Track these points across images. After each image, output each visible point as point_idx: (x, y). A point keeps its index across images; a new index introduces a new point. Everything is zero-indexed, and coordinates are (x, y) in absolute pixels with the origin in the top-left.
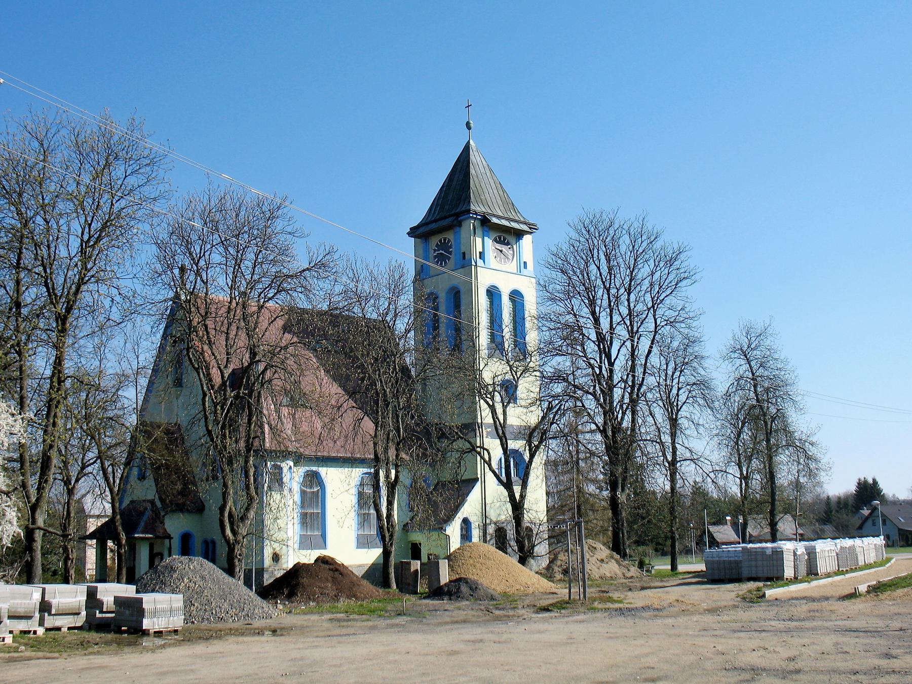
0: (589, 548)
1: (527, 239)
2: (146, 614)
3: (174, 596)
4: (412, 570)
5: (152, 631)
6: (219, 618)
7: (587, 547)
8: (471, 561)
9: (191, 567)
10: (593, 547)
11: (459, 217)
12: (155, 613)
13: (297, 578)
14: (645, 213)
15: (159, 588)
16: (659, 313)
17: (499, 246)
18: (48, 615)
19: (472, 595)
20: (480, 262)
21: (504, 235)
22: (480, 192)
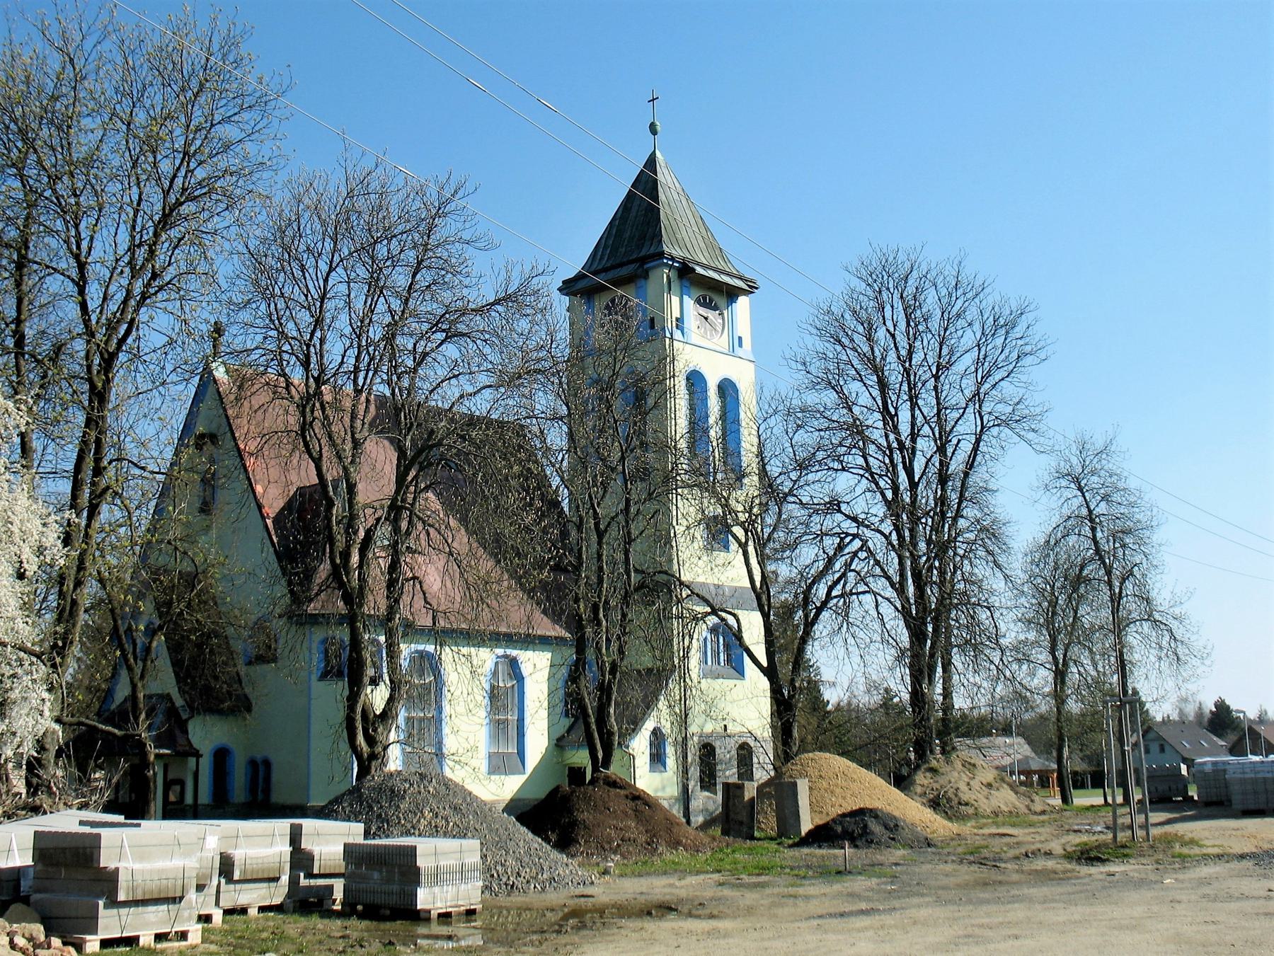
0: (963, 765)
1: (743, 301)
2: (423, 879)
3: (464, 842)
4: (746, 799)
5: (434, 914)
6: (506, 884)
8: (825, 784)
9: (431, 790)
10: (970, 764)
12: (438, 877)
13: (570, 812)
14: (962, 253)
15: (379, 828)
16: (987, 407)
17: (703, 311)
18: (227, 883)
19: (893, 839)
20: (677, 335)
21: (710, 294)
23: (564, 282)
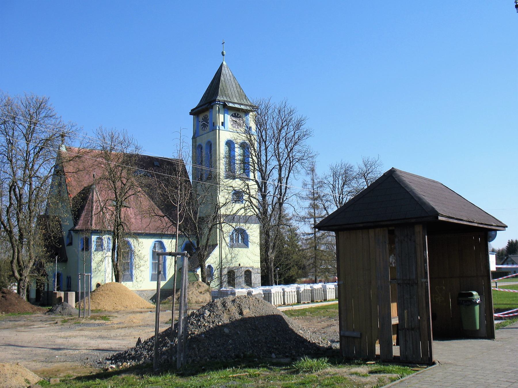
4: (57, 297)
7: (196, 284)
11: (211, 104)
14: (286, 99)
17: (234, 119)
20: (222, 128)
22: (225, 89)
23: (192, 110)
